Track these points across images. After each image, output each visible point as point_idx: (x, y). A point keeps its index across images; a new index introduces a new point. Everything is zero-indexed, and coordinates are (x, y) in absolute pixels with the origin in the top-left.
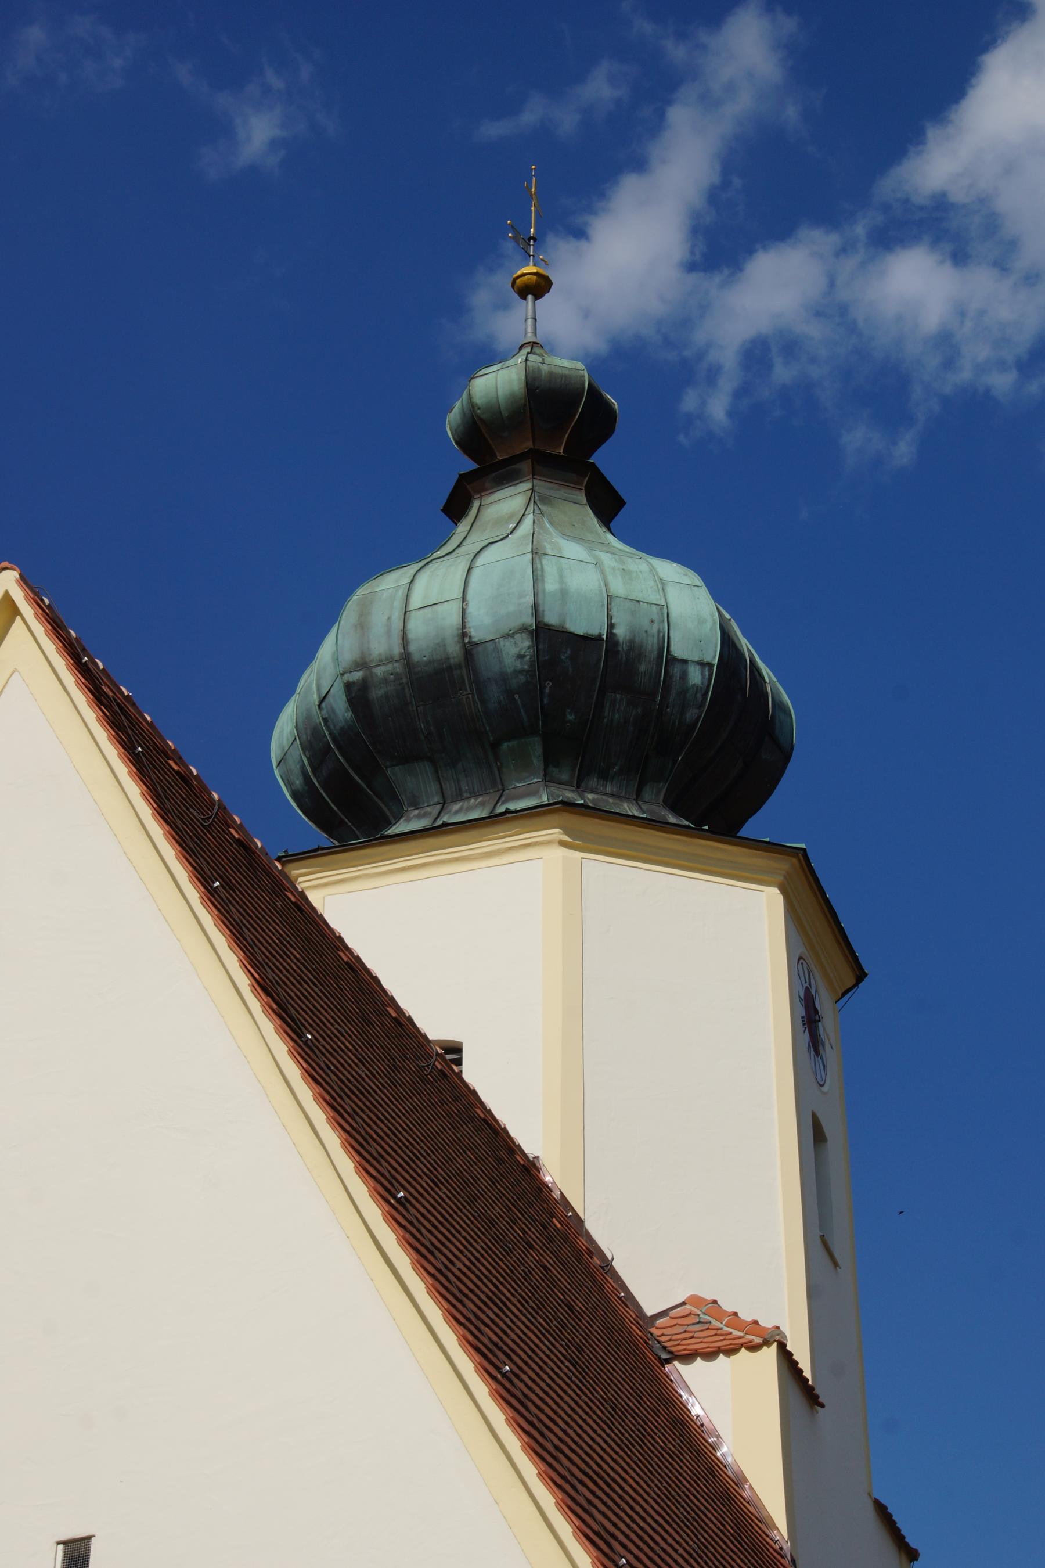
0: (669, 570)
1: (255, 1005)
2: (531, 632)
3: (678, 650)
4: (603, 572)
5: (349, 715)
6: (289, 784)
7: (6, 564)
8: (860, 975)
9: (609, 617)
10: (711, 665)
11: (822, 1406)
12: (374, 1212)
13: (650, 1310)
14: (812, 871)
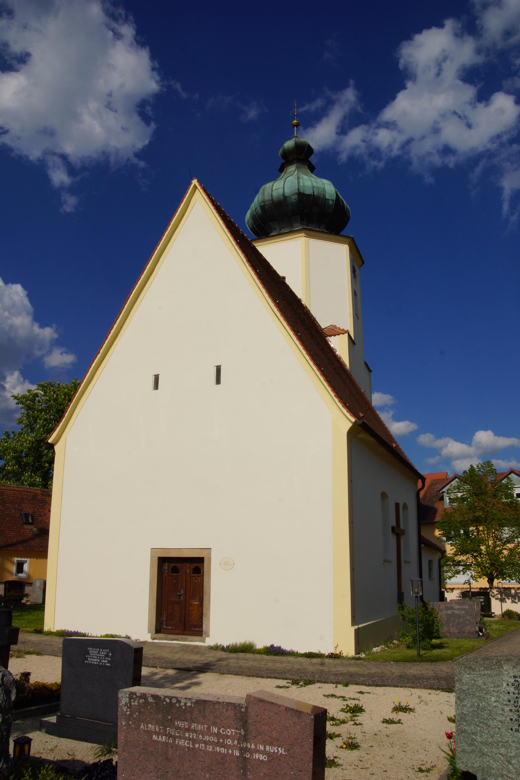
0: (325, 181)
1: (247, 264)
3: (327, 197)
4: (312, 182)
5: (261, 212)
6: (249, 227)
7: (194, 178)
8: (363, 263)
9: (313, 191)
10: (334, 200)
11: (356, 344)
12: (272, 305)
13: (323, 328)
14: (354, 241)
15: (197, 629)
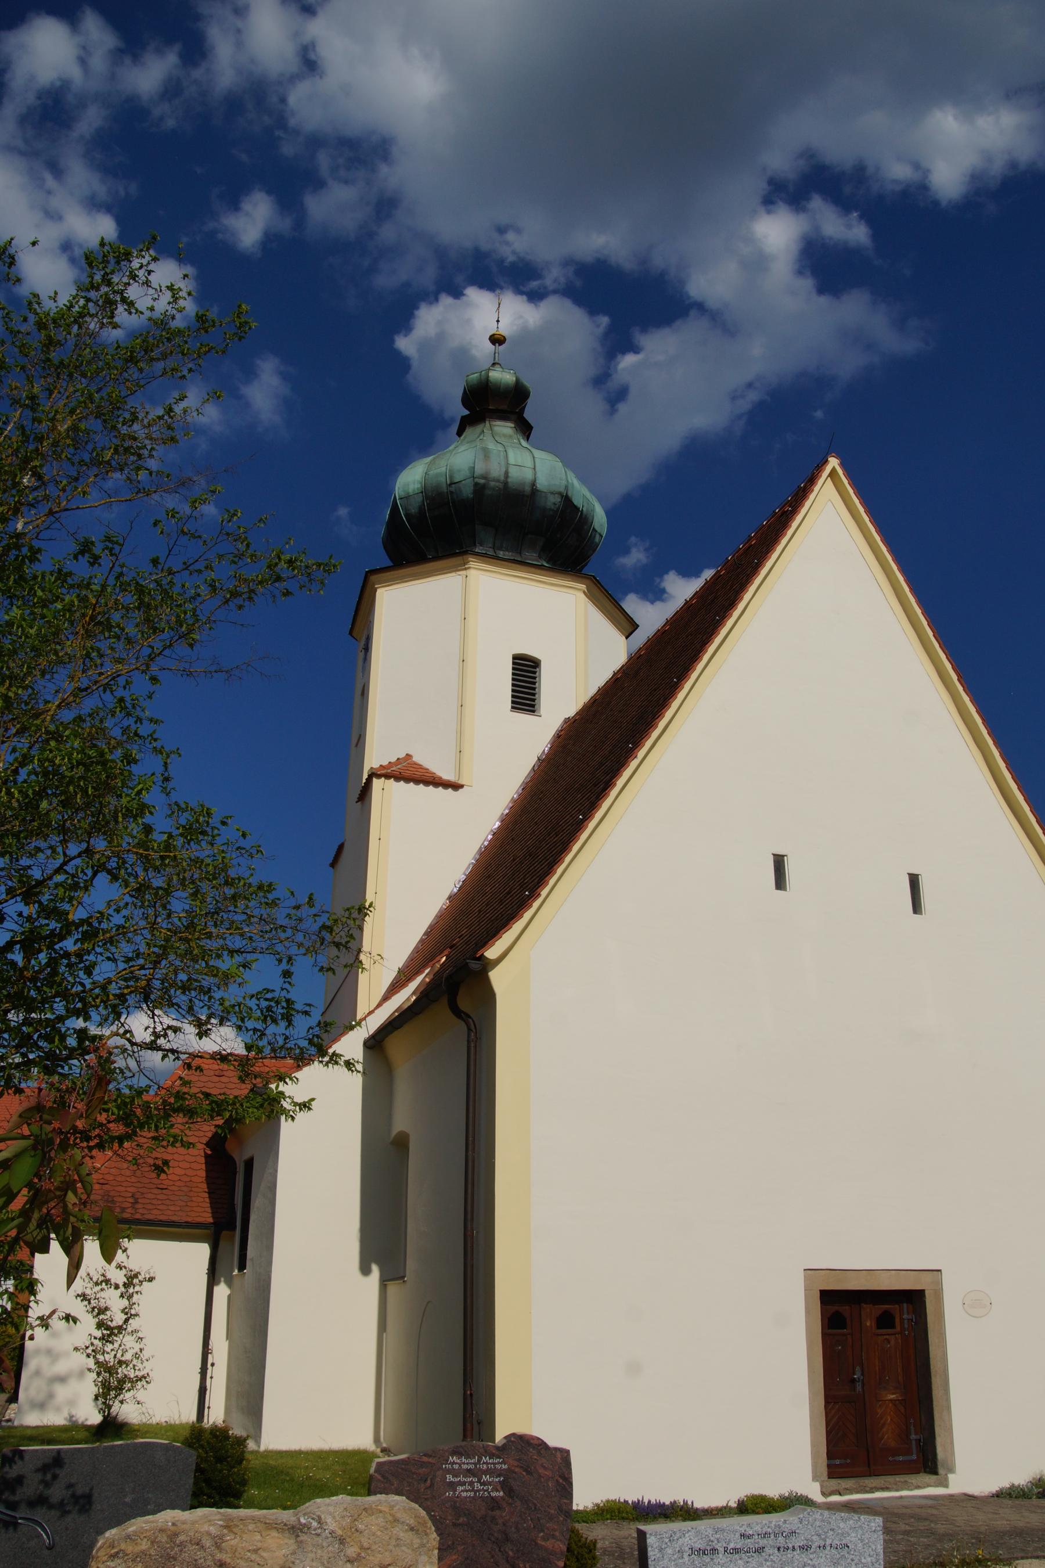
2: (562, 496)
15: (901, 1458)
